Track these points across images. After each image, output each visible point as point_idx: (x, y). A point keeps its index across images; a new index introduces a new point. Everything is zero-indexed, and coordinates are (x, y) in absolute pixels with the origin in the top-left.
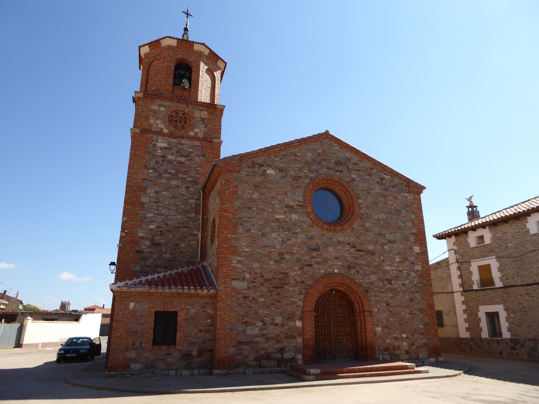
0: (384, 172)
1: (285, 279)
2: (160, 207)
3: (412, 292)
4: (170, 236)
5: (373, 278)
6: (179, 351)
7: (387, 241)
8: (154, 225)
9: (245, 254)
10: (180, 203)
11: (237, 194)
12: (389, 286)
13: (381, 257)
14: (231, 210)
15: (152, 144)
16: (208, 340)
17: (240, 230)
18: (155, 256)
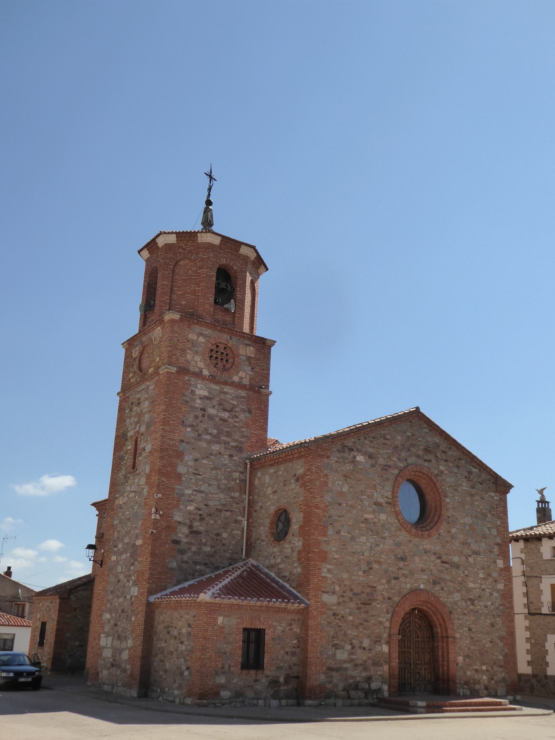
0: (472, 464)
1: (373, 594)
2: (200, 481)
3: (494, 616)
4: (211, 522)
5: (457, 596)
6: (266, 676)
7: (472, 551)
8: (193, 505)
9: (335, 561)
10: (222, 476)
11: (327, 486)
12: (472, 607)
13: (465, 571)
14: (322, 506)
15: (190, 391)
16: (295, 665)
17: (330, 531)
18: (194, 549)
